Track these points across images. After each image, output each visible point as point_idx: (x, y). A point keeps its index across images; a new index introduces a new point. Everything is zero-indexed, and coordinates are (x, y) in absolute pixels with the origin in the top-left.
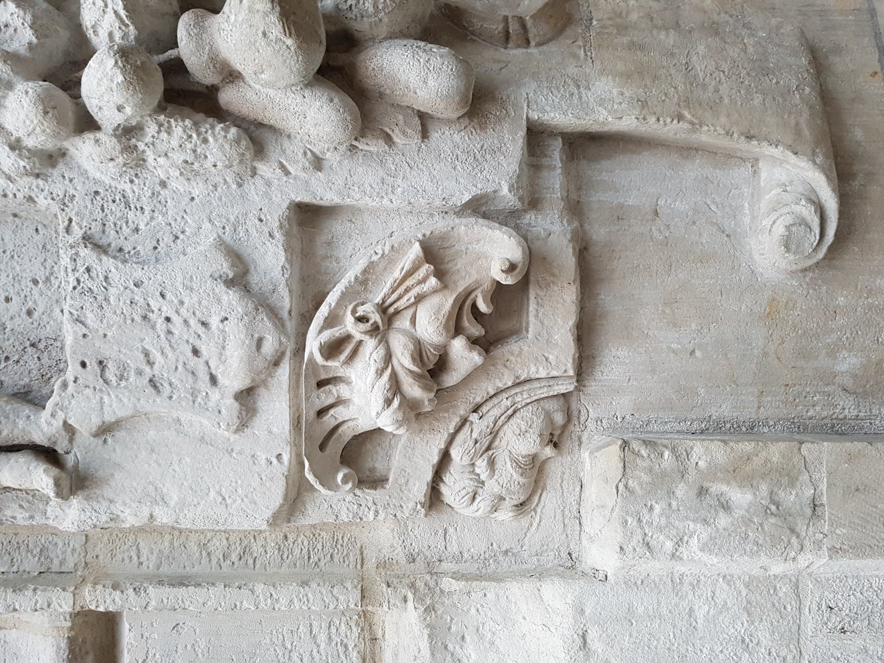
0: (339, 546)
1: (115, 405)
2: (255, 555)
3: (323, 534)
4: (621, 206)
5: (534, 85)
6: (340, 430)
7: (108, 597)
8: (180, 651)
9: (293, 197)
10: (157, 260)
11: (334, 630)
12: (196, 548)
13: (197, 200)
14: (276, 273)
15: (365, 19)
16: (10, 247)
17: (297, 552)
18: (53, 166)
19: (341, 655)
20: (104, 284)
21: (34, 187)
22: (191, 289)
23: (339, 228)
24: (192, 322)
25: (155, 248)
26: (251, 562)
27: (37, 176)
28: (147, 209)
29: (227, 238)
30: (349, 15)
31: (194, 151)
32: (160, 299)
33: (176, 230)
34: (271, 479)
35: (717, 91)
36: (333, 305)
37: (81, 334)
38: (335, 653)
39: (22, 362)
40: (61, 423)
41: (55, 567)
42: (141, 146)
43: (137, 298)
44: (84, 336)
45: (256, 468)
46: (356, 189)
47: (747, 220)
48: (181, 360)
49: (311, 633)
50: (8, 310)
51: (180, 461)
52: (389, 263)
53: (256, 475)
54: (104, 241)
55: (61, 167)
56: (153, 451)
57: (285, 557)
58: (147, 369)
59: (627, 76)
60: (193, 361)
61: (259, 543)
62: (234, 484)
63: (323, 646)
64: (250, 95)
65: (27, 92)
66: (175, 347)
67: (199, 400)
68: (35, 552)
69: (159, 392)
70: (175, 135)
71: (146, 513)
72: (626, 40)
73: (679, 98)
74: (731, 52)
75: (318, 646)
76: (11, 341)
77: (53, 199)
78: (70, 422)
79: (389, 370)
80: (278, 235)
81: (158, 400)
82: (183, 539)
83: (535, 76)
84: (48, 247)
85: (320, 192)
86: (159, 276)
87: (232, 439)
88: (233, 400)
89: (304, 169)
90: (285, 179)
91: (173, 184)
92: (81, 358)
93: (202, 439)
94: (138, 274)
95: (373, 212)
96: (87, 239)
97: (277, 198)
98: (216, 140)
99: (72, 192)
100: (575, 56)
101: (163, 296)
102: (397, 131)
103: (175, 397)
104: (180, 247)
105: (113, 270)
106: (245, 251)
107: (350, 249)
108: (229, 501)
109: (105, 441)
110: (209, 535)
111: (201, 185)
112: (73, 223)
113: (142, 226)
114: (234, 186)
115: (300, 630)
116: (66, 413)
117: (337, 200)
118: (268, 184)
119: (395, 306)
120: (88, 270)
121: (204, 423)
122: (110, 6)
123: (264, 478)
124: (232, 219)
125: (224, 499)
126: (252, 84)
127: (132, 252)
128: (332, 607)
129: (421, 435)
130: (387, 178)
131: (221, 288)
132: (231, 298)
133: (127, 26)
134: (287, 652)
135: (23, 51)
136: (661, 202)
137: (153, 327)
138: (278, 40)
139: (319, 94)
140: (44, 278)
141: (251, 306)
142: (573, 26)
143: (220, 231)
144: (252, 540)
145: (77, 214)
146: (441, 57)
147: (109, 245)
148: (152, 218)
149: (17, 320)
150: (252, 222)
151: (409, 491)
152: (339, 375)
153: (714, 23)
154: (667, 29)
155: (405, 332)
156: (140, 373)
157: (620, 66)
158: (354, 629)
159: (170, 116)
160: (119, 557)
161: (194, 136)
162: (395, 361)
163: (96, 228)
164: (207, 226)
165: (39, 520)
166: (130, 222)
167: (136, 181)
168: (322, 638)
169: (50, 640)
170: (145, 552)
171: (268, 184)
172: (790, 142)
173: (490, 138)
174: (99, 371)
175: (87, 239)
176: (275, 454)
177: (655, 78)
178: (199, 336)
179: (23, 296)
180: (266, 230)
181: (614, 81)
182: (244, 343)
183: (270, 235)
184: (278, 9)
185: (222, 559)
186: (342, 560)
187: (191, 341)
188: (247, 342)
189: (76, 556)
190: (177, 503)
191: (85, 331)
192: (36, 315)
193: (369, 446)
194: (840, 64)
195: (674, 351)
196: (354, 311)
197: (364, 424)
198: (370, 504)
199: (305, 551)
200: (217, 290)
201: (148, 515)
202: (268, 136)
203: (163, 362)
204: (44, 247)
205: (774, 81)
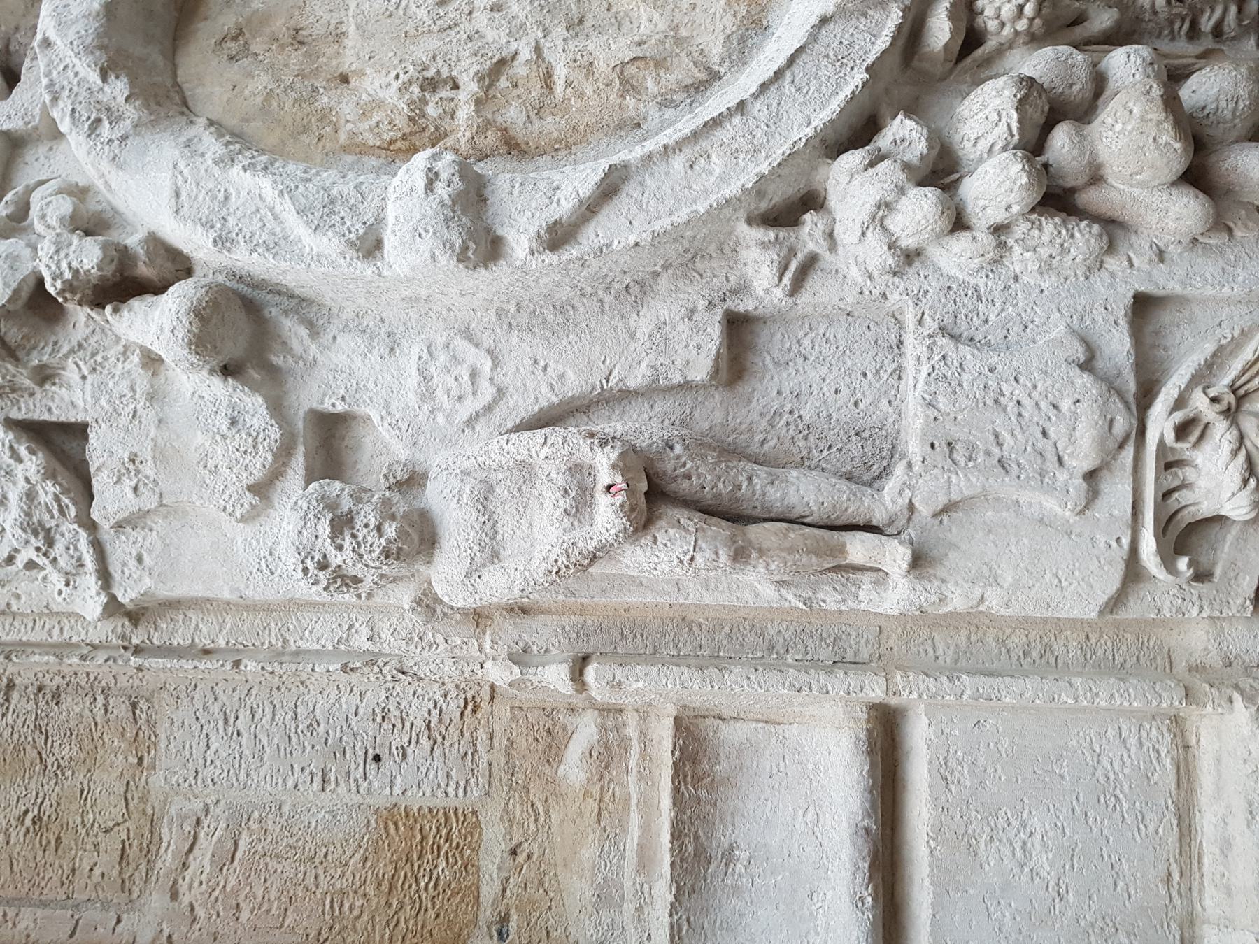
0: (1145, 649)
1: (962, 484)
2: (1056, 654)
3: (1128, 635)
6: (1179, 516)
7: (921, 683)
8: (982, 750)
9: (1137, 286)
10: (1008, 348)
11: (1144, 734)
12: (994, 644)
13: (1046, 292)
15: (1221, 125)
16: (842, 343)
17: (1100, 652)
18: (910, 265)
19: (1154, 761)
20: (959, 370)
21: (890, 284)
22: (1046, 373)
24: (1043, 405)
25: (1006, 337)
26: (1052, 660)
27: (895, 274)
28: (998, 303)
29: (1075, 325)
30: (1205, 122)
31: (1062, 245)
32: (1014, 384)
33: (1026, 319)
34: (1110, 563)
36: (1183, 387)
37: (933, 417)
38: (1147, 758)
39: (844, 451)
40: (907, 501)
41: (850, 656)
42: (1011, 242)
43: (990, 383)
44: (935, 419)
45: (1095, 551)
46: (1198, 278)
49: (1120, 736)
50: (836, 401)
51: (1017, 542)
52: (1237, 346)
53: (1095, 558)
54: (956, 332)
55: (917, 264)
56: (990, 531)
57: (1088, 657)
58: (996, 450)
60: (1041, 443)
61: (1061, 642)
62: (1071, 567)
63: (1133, 750)
64: (1113, 195)
66: (1025, 428)
67: (1047, 480)
68: (828, 641)
69: (1007, 471)
70: (1046, 230)
71: (977, 592)
75: (1129, 750)
76: (836, 431)
77: (908, 295)
78: (913, 501)
79: (1243, 452)
80: (1122, 322)
81: (1007, 479)
82: (980, 634)
84: (880, 342)
85: (1162, 282)
86: (1014, 362)
87: (1071, 521)
88: (1081, 481)
89: (1150, 260)
90: (1129, 271)
91: (1025, 278)
92: (931, 440)
93: (1041, 521)
94: (994, 359)
95: (1202, 302)
97: (1121, 289)
98: (1083, 235)
99: (926, 287)
101: (1016, 380)
102: (1239, 223)
103: (1022, 477)
104: (1030, 336)
105: (969, 357)
107: (1179, 337)
108: (1064, 584)
109: (941, 522)
110: (1008, 632)
111: (1053, 278)
112: (926, 316)
113: (992, 318)
114: (1082, 279)
115: (1108, 733)
116: (913, 492)
117: (1178, 289)
118: (1113, 275)
119: (1245, 388)
120: (944, 357)
121: (1051, 505)
122: (1004, 120)
123: (1102, 561)
124: (1080, 308)
125: (1060, 582)
126: (1115, 185)
127: (983, 341)
128: (1155, 703)
129: (1255, 527)
130: (1226, 267)
132: (1084, 380)
133: (1012, 136)
134: (1096, 755)
135: (915, 161)
137: (1004, 410)
138: (1167, 143)
139: (1185, 192)
140: (874, 371)
141: (1104, 388)
143: (1069, 320)
144: (1053, 638)
145: (931, 307)
147: (961, 335)
148: (1003, 310)
149: (844, 410)
151: (1238, 586)
152: (1185, 457)
156: (988, 453)
158: (1166, 734)
159: (1041, 215)
160: (914, 650)
161: (1064, 232)
162: (1248, 443)
163: (948, 320)
165: (851, 603)
166: (981, 314)
167: (991, 275)
168: (1132, 741)
169: (846, 732)
170: (941, 647)
171: (1113, 275)
174: (948, 452)
176: (1115, 537)
178: (1049, 418)
179: (852, 388)
180: (1112, 318)
182: (1097, 423)
183: (1115, 323)
184: (1171, 117)
185: (1022, 656)
186: (1148, 663)
187: (1041, 423)
188: (1100, 423)
189: (870, 647)
190: (1011, 585)
191: (936, 413)
192: (862, 406)
193: (1194, 538)
197: (1206, 509)
198: (1195, 598)
199: (1109, 652)
200: (1071, 374)
201: (980, 596)
202: (1118, 232)
203: (1012, 442)
204: (876, 342)
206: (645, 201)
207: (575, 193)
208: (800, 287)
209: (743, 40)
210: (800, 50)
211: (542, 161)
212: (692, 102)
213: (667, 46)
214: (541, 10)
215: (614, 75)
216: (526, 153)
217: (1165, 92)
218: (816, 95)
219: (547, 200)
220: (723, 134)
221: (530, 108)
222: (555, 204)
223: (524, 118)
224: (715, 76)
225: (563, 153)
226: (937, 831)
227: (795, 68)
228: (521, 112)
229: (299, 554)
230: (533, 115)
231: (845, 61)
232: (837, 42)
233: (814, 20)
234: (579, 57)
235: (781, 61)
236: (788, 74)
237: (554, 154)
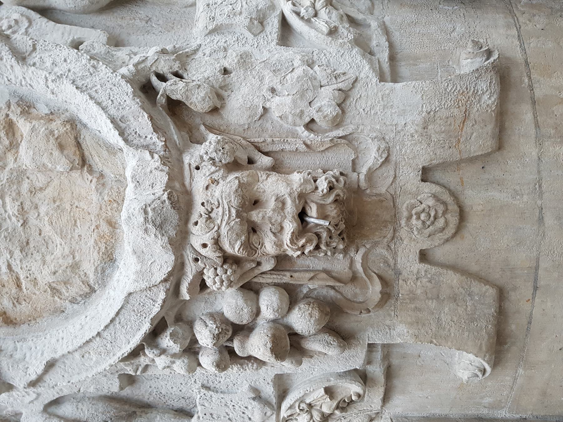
4: (405, 353)
5: (371, 330)
14: (271, 393)
23: (273, 252)
29: (253, 385)
35: (449, 330)
47: (456, 359)
48: (239, 414)
54: (209, 385)
58: (228, 416)
59: (411, 324)
65: (182, 368)
72: (413, 306)
73: (432, 335)
74: (459, 311)
80: (271, 383)
83: (372, 326)
96: (203, 386)
100: (390, 315)
106: (259, 388)
131: (252, 401)
132: (255, 403)
136: (422, 352)
137: (229, 407)
142: (390, 300)
143: (250, 383)
146: (334, 348)
150: (261, 380)
153: (455, 294)
154: (432, 299)
155: (317, 410)
157: (409, 320)
161: (242, 370)
163: (205, 382)
164: (245, 382)
172: (476, 353)
173: (352, 352)
175: (203, 386)
177: (424, 324)
181: (406, 326)
184: (274, 356)
194: (513, 296)
195: (420, 397)
196: (299, 406)
205: (476, 325)
206: (67, 369)
207: (35, 373)
208: (147, 370)
209: (103, 271)
210: (120, 310)
211: (24, 327)
212: (85, 302)
213: (68, 273)
214: (6, 240)
215: (47, 287)
216: (16, 324)
217: (272, 346)
218: (130, 330)
219: (24, 374)
220: (93, 345)
221: (13, 299)
222: (28, 375)
223: (12, 305)
224: (93, 290)
225: (33, 322)
226: (286, 339)
227: (120, 316)
228: (10, 301)
229: (29, 227)
230: (15, 302)
231: (142, 313)
232: (138, 304)
233: (125, 294)
234: (29, 276)
235: (112, 315)
236: (117, 319)
237: (29, 323)
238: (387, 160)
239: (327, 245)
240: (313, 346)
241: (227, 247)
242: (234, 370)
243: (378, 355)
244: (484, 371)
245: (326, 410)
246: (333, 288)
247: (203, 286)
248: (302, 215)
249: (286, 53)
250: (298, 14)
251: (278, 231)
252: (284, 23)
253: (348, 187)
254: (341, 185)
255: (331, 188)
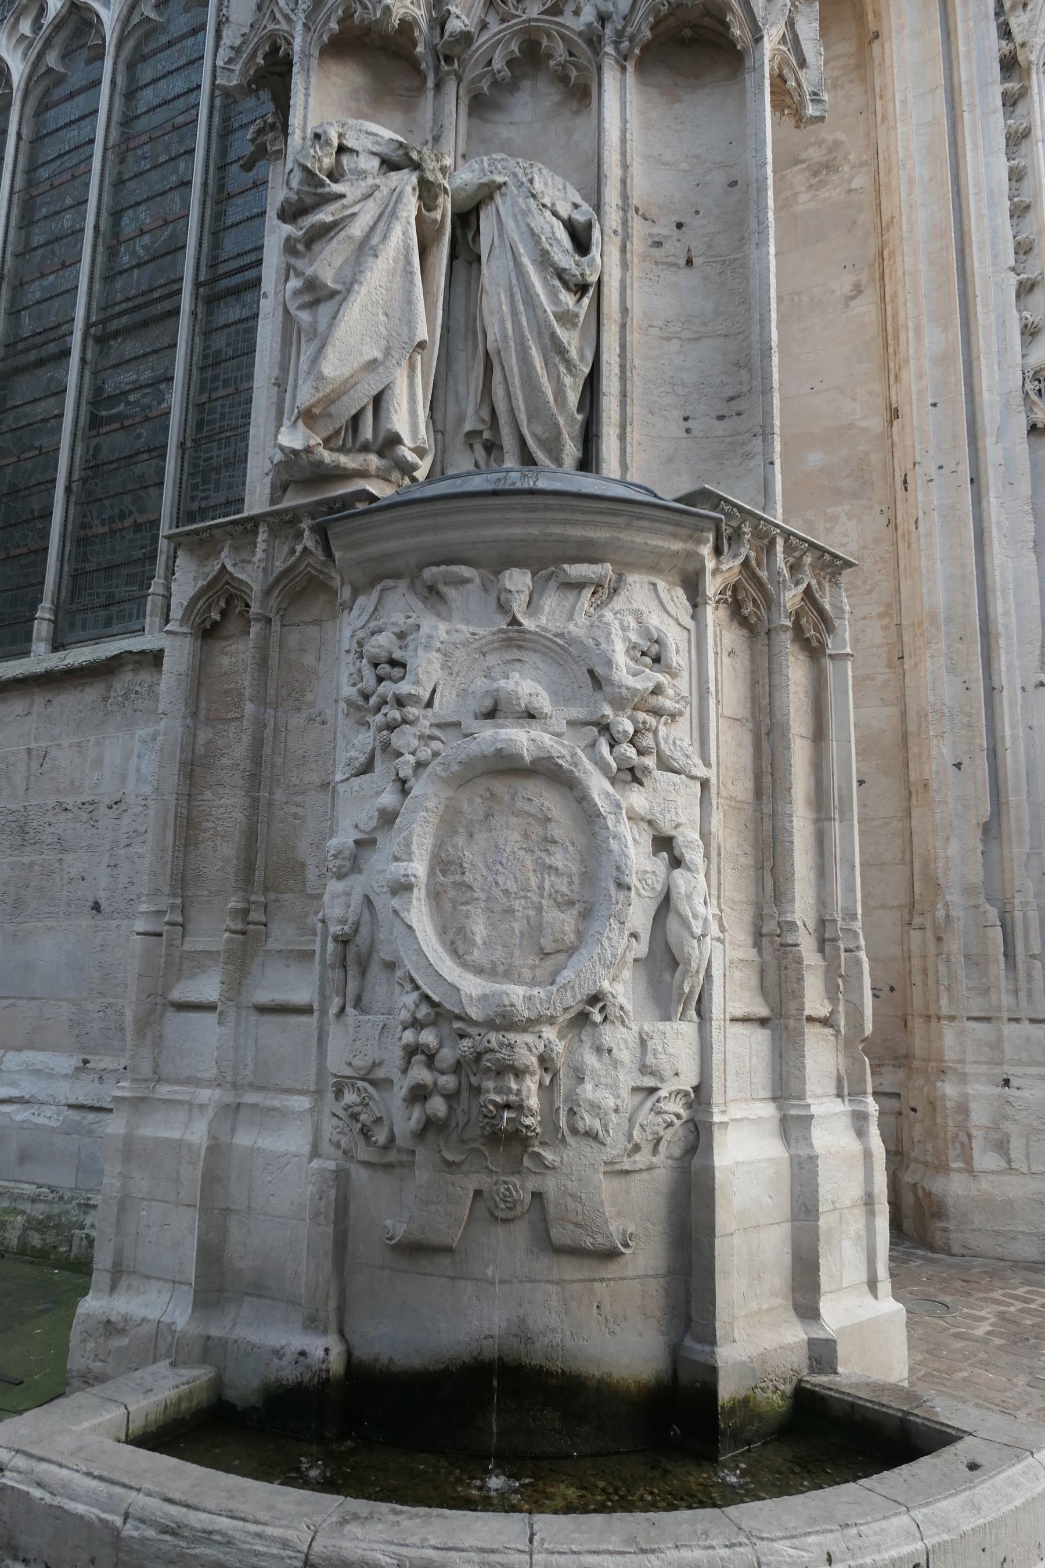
132: (370, 1063)
175: (385, 1025)
238: (547, 1167)
239: (487, 1123)
240: (417, 1113)
241: (488, 1056)
242: (399, 1053)
243: (405, 1158)
244: (390, 1239)
245: (363, 1117)
246: (457, 1125)
247: (462, 1036)
248: (508, 1106)
249: (625, 1093)
250: (658, 1101)
251: (498, 1091)
252: (653, 1090)
253: (528, 1138)
254: (529, 1134)
255: (527, 1127)
